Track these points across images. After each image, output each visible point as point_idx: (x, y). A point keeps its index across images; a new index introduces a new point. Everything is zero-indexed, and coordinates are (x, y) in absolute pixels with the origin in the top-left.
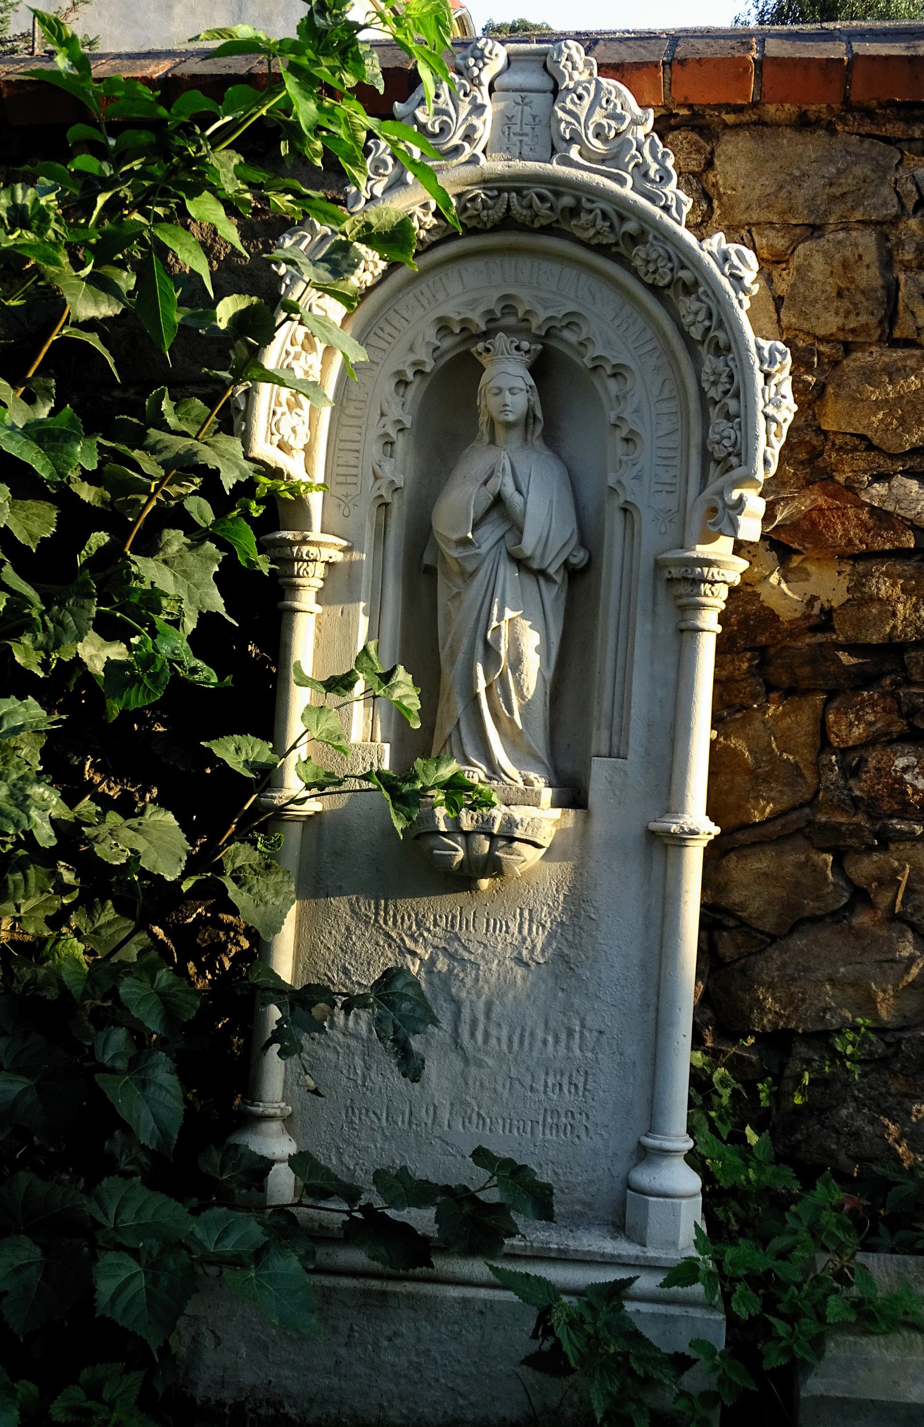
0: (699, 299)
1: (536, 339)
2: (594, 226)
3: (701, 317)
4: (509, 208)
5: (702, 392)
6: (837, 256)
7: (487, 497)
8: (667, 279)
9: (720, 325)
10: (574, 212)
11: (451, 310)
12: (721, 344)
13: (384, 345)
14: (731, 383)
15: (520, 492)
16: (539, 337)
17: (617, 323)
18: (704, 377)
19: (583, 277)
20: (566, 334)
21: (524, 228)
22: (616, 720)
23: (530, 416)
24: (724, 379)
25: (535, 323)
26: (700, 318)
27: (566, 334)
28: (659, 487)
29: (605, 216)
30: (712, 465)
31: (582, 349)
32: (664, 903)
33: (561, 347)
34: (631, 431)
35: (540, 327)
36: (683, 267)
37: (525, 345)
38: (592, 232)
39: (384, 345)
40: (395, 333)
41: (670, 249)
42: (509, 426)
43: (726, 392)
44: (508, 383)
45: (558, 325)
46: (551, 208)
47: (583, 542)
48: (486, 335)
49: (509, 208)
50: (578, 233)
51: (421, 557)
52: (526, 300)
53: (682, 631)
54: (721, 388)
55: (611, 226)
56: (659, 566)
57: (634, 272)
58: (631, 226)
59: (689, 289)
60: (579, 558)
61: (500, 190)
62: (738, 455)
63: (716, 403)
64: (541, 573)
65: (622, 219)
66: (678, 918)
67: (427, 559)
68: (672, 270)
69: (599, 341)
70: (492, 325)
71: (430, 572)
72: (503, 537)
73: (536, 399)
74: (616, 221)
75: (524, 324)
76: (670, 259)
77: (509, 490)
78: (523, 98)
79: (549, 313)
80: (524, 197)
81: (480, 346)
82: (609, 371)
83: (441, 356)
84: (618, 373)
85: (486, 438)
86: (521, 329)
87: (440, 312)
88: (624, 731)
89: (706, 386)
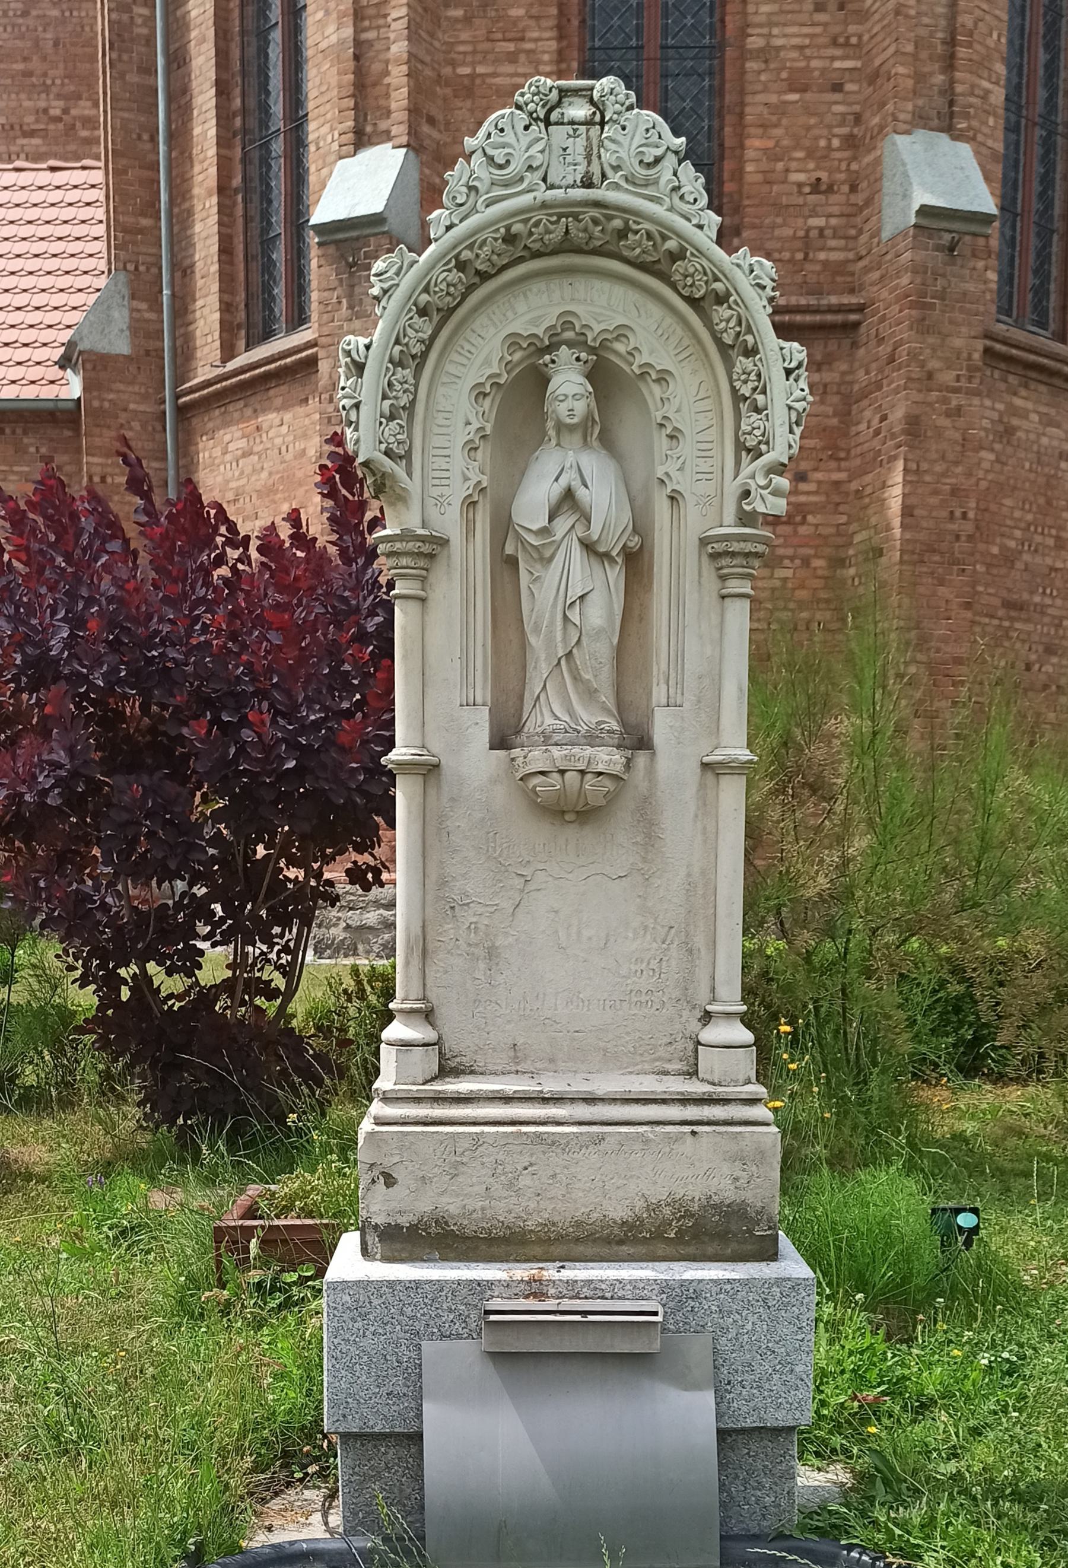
0: (730, 308)
1: (592, 350)
2: (640, 245)
4: (567, 232)
5: (734, 390)
6: (884, 294)
8: (702, 292)
9: (749, 330)
10: (622, 234)
11: (520, 326)
12: (750, 346)
13: (465, 361)
14: (759, 380)
15: (586, 487)
16: (594, 348)
17: (660, 332)
18: (735, 377)
19: (630, 292)
20: (620, 347)
21: (579, 251)
22: (672, 675)
23: (588, 418)
24: (753, 377)
26: (731, 325)
27: (620, 347)
28: (700, 476)
30: (744, 453)
31: (631, 359)
32: (615, 1100)
33: (613, 358)
34: (675, 429)
35: (594, 339)
36: (717, 279)
37: (583, 355)
38: (638, 251)
39: (465, 361)
40: (473, 350)
41: (705, 263)
42: (572, 428)
43: (755, 389)
44: (569, 386)
45: (609, 336)
47: (635, 531)
48: (550, 349)
49: (567, 232)
50: (626, 253)
51: (503, 548)
53: (723, 597)
54: (750, 385)
56: (704, 542)
57: (673, 286)
58: (672, 244)
59: (721, 299)
60: (635, 542)
61: (560, 216)
62: (767, 443)
63: (746, 399)
65: (665, 238)
67: (509, 549)
68: (706, 283)
69: (644, 349)
70: (555, 339)
71: (512, 562)
72: (573, 526)
73: (593, 404)
75: (582, 338)
76: (705, 274)
77: (576, 484)
78: (575, 130)
79: (603, 326)
80: (580, 221)
81: (547, 358)
83: (512, 369)
84: (663, 377)
85: (554, 442)
86: (579, 343)
88: (680, 683)
89: (737, 384)
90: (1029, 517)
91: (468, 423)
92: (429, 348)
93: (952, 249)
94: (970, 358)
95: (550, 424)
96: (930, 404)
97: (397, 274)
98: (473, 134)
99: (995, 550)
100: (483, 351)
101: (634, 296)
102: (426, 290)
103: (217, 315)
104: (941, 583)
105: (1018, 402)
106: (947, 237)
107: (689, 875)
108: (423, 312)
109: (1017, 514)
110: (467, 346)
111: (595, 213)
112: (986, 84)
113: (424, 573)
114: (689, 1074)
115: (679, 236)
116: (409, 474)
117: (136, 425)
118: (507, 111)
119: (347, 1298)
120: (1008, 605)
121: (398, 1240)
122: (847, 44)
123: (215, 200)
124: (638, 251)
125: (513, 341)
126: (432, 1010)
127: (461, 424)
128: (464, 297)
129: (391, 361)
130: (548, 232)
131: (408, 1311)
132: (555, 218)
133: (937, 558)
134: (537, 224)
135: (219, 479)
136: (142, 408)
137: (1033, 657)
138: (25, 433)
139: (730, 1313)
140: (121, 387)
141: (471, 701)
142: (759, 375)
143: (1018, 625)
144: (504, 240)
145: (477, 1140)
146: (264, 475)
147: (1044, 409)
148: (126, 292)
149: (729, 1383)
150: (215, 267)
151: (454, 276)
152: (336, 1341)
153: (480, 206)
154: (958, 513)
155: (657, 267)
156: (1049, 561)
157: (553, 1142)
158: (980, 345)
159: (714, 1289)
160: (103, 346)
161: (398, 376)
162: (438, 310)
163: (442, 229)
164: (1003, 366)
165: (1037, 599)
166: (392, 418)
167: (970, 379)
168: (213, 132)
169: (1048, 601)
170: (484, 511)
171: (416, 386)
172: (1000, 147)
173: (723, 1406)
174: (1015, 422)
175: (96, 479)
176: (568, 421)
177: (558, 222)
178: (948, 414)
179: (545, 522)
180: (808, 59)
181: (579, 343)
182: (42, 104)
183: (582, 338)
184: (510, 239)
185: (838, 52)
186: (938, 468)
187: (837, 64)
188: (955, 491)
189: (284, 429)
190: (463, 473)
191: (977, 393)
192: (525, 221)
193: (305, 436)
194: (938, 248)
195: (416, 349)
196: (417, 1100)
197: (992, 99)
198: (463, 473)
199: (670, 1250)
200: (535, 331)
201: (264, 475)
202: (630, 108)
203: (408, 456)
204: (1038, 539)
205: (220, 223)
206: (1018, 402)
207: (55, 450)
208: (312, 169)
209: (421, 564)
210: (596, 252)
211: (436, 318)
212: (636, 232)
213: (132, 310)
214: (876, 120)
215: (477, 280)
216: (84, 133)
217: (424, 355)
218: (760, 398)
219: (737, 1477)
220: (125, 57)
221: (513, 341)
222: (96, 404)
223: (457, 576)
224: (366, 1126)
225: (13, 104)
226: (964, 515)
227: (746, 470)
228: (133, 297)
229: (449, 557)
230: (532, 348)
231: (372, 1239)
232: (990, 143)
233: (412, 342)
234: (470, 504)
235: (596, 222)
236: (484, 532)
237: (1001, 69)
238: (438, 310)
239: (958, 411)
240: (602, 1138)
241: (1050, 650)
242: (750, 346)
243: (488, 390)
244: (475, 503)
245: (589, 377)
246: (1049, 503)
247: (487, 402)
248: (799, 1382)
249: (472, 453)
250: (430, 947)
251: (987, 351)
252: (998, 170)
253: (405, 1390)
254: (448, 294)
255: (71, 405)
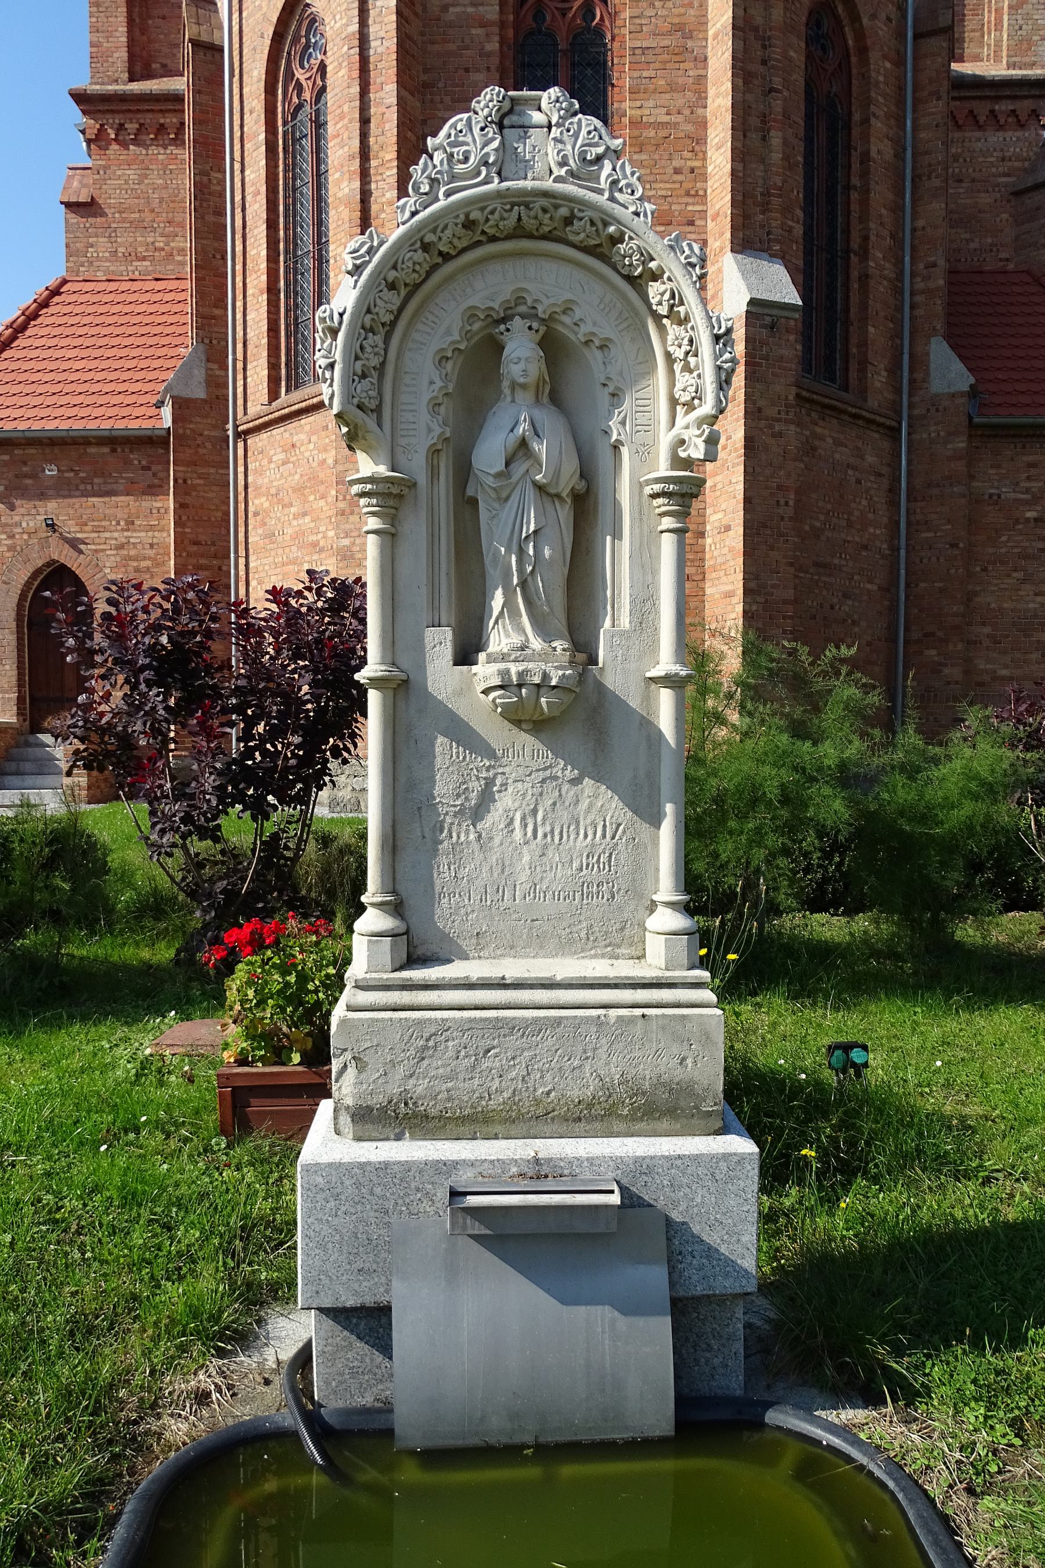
3: (667, 296)
4: (519, 219)
7: (655, 256)
10: (568, 221)
12: (682, 316)
16: (544, 320)
17: (602, 306)
20: (565, 319)
21: (530, 236)
25: (540, 309)
27: (565, 319)
29: (592, 223)
31: (576, 328)
33: (560, 328)
34: (617, 388)
38: (582, 235)
42: (524, 387)
44: (521, 354)
45: (558, 310)
46: (551, 218)
47: (582, 476)
48: (503, 320)
49: (519, 219)
50: (572, 238)
52: (534, 290)
55: (597, 230)
60: (582, 486)
61: (513, 205)
62: (700, 399)
64: (558, 496)
65: (606, 224)
66: (677, 727)
67: (470, 492)
70: (510, 312)
73: (544, 366)
74: (600, 226)
75: (533, 311)
79: (552, 301)
81: (502, 327)
82: (597, 343)
83: (472, 337)
85: (509, 399)
86: (531, 315)
87: (471, 302)
90: (829, 506)
91: (432, 383)
92: (397, 318)
93: (772, 328)
94: (786, 398)
95: (506, 384)
96: (761, 430)
97: (368, 252)
98: (434, 135)
99: (807, 528)
100: (444, 325)
101: (578, 275)
102: (394, 267)
103: (266, 372)
104: (772, 548)
105: (818, 430)
106: (768, 319)
107: (635, 777)
108: (392, 286)
109: (821, 504)
110: (431, 317)
111: (544, 202)
112: (790, 223)
113: (393, 511)
114: (638, 958)
115: (620, 223)
116: (380, 425)
117: (208, 445)
118: (465, 116)
119: (320, 1180)
120: (816, 564)
121: (371, 1119)
122: (697, 195)
123: (265, 296)
124: (582, 235)
125: (471, 315)
126: (401, 902)
127: (425, 383)
128: (429, 274)
129: (363, 328)
130: (502, 219)
131: (378, 1190)
132: (508, 207)
133: (769, 532)
134: (492, 212)
135: (266, 480)
136: (213, 433)
137: (835, 600)
138: (131, 451)
139: (680, 1187)
140: (198, 419)
141: (436, 623)
142: (691, 341)
143: (824, 579)
144: (464, 226)
145: (444, 1027)
146: (297, 477)
147: (835, 435)
148: (203, 357)
149: (680, 1253)
150: (265, 341)
151: (419, 256)
152: (309, 1221)
153: (441, 195)
154: (782, 502)
155: (599, 250)
156: (843, 536)
157: (512, 1027)
158: (794, 390)
159: (666, 1165)
160: (186, 393)
161: (370, 341)
162: (406, 285)
163: (407, 214)
164: (807, 405)
165: (836, 561)
166: (364, 376)
167: (787, 413)
168: (264, 253)
169: (843, 562)
170: (447, 458)
171: (386, 350)
172: (800, 263)
173: (675, 1276)
174: (817, 443)
175: (180, 481)
176: (522, 380)
177: (511, 210)
178: (773, 435)
179: (500, 466)
180: (670, 204)
181: (531, 315)
182: (150, 240)
183: (533, 311)
184: (469, 224)
185: (690, 200)
186: (767, 472)
187: (690, 208)
188: (780, 487)
189: (311, 446)
190: (396, 262)
191: (791, 422)
192: (482, 209)
193: (326, 450)
194: (762, 326)
195: (387, 318)
196: (387, 987)
197: (795, 231)
198: (396, 262)
199: (622, 1127)
200: (492, 304)
201: (297, 477)
202: (575, 114)
203: (378, 410)
204: (834, 520)
205: (268, 312)
206: (818, 430)
207: (152, 463)
208: (332, 274)
209: (392, 503)
210: (544, 237)
211: (403, 292)
212: (581, 219)
213: (207, 369)
214: (718, 244)
215: (440, 260)
216: (179, 258)
217: (393, 324)
218: (692, 360)
219: (687, 1340)
220: (205, 204)
221: (471, 315)
222: (181, 431)
223: (423, 514)
224: (339, 1012)
225: (131, 240)
226: (787, 504)
227: (681, 420)
228: (208, 361)
229: (416, 497)
230: (490, 320)
231: (345, 1119)
232: (794, 260)
233: (382, 312)
234: (435, 452)
235: (545, 210)
236: (447, 476)
237: (800, 213)
238: (406, 285)
239: (780, 434)
240: (559, 1021)
241: (846, 596)
242: (682, 316)
243: (449, 355)
244: (438, 451)
245: (540, 344)
246: (842, 496)
247: (450, 365)
248: (745, 1252)
249: (436, 409)
250: (399, 843)
251: (798, 395)
252: (800, 278)
253: (375, 1267)
254: (414, 271)
255: (164, 433)
